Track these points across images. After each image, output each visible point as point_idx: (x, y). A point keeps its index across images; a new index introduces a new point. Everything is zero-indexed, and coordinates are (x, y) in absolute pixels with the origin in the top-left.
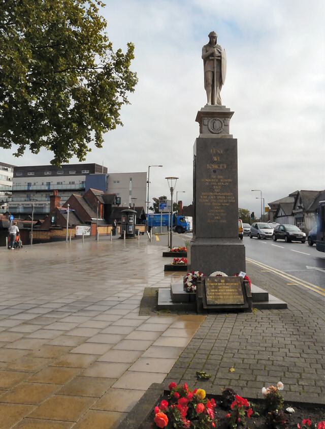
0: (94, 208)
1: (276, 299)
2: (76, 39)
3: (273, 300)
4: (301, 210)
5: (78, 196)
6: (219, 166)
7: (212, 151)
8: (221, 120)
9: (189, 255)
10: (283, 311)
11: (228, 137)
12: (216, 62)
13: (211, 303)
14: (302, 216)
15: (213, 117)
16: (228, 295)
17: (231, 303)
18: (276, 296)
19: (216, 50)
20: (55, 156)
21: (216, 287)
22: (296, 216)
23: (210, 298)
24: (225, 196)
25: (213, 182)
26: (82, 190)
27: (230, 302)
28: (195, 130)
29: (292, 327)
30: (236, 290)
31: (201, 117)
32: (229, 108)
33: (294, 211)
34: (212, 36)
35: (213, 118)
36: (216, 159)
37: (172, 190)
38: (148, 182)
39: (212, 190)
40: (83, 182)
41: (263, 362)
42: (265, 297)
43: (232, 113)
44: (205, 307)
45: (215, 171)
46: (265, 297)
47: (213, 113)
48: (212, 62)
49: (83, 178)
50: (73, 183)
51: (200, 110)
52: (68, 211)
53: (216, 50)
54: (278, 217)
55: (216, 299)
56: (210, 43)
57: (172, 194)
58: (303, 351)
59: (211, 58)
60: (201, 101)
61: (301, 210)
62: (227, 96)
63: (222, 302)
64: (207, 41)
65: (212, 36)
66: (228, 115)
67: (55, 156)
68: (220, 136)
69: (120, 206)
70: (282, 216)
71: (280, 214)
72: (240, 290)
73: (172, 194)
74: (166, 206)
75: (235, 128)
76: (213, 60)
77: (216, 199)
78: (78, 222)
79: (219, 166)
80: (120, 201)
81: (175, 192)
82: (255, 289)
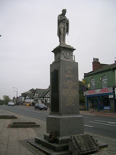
4: (37, 97)
8: (70, 52)
12: (66, 24)
14: (37, 99)
15: (66, 50)
20: (45, 137)
22: (34, 99)
25: (68, 84)
28: (52, 58)
31: (57, 51)
32: (72, 45)
33: (34, 97)
45: (69, 78)
48: (64, 23)
59: (64, 21)
60: (57, 44)
64: (61, 13)
65: (64, 11)
66: (72, 50)
67: (45, 137)
68: (69, 60)
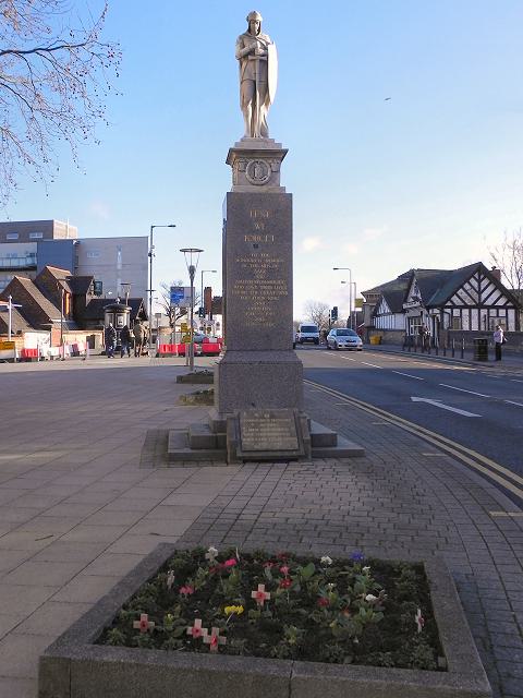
0: (57, 302)
1: (350, 443)
2: (133, 336)
3: (345, 444)
5: (25, 280)
6: (263, 238)
7: (253, 214)
9: (216, 377)
10: (358, 460)
11: (278, 192)
12: (257, 63)
13: (248, 448)
15: (253, 158)
16: (275, 435)
17: (278, 448)
18: (349, 438)
19: (259, 46)
21: (256, 425)
22: (407, 315)
23: (247, 441)
24: (273, 285)
26: (32, 268)
27: (278, 446)
29: (366, 479)
30: (287, 430)
34: (252, 20)
35: (256, 158)
36: (258, 227)
37: (192, 270)
38: (150, 255)
39: (252, 275)
40: (32, 256)
41: (313, 522)
42: (332, 440)
43: (285, 152)
44: (239, 454)
45: (256, 246)
46: (332, 440)
47: (253, 152)
49: (32, 247)
50: (15, 257)
51: (232, 147)
52: (10, 307)
53: (259, 46)
54: (379, 316)
55: (256, 442)
56: (249, 30)
57: (192, 278)
58: (437, 546)
60: (235, 132)
61: (418, 304)
62: (280, 121)
63: (264, 446)
69: (102, 297)
70: (385, 314)
71: (381, 311)
72: (293, 428)
73: (192, 278)
74: (182, 297)
75: (290, 177)
76: (253, 62)
77: (258, 290)
78: (24, 323)
79: (263, 238)
80: (101, 288)
81: (197, 275)
82: (319, 429)
